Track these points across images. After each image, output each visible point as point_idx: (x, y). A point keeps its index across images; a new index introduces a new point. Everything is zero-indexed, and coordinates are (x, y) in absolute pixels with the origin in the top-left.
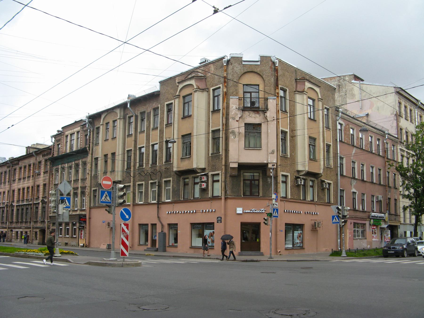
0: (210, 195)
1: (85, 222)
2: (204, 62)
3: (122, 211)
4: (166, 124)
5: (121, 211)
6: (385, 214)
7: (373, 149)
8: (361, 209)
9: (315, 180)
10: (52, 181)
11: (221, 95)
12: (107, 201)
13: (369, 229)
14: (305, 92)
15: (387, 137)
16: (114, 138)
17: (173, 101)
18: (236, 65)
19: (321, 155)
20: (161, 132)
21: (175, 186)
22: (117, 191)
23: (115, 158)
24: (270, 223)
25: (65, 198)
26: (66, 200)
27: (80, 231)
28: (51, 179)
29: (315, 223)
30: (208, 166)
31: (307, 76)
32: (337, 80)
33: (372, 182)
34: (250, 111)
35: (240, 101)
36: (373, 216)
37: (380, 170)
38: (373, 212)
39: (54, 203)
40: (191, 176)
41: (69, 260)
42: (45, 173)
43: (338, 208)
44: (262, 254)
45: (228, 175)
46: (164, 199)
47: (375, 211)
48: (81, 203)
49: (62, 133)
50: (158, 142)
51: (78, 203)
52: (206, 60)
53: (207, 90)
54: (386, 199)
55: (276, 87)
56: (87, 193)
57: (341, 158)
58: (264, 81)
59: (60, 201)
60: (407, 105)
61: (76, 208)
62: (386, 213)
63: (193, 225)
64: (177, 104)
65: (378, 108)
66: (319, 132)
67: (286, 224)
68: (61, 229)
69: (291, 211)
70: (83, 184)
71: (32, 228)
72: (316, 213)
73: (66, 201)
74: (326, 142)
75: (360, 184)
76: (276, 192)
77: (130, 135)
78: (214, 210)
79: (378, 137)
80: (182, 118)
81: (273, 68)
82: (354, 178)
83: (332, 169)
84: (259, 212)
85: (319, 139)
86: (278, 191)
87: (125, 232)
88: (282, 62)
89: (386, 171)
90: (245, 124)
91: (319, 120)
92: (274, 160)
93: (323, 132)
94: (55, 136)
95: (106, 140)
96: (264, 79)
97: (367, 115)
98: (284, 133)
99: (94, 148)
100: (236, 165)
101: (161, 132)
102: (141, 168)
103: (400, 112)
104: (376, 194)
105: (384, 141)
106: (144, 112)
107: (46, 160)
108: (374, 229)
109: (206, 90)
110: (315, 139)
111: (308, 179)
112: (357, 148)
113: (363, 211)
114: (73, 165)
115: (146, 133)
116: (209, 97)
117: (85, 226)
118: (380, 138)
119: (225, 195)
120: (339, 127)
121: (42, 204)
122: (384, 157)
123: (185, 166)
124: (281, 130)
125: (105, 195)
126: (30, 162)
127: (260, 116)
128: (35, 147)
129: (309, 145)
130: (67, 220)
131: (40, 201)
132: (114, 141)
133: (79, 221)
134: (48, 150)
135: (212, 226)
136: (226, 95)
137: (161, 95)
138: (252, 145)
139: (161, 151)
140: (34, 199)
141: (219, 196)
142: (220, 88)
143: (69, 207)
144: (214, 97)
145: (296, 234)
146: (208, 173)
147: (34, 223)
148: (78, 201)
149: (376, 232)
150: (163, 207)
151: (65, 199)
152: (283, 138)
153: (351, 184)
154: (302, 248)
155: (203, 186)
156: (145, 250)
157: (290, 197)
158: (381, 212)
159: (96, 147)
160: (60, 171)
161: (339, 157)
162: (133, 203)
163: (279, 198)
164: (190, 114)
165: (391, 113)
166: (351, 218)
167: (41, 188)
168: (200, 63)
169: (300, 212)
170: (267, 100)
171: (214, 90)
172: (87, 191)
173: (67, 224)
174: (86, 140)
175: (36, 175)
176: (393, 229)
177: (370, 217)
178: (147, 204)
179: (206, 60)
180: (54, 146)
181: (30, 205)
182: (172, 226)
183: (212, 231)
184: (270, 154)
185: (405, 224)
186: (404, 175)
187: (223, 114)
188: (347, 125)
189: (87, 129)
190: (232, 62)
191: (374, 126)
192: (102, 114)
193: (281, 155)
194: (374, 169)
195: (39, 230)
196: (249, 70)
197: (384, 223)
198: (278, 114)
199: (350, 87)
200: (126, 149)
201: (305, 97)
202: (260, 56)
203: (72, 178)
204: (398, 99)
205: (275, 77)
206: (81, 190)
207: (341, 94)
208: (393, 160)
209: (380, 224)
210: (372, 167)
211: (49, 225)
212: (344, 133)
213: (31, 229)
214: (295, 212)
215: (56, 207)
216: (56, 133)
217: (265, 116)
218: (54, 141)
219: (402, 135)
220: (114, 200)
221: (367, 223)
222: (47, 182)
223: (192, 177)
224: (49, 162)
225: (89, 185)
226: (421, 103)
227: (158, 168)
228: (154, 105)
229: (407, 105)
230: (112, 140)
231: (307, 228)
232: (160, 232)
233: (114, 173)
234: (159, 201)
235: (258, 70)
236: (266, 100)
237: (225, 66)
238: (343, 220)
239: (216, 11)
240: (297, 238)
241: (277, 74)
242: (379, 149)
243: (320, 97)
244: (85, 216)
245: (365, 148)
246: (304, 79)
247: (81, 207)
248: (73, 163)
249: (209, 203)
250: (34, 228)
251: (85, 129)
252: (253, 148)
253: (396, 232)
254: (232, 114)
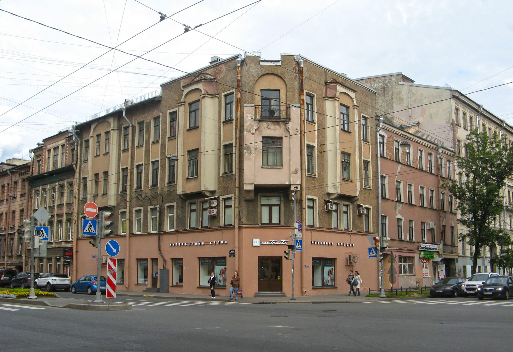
0: (222, 224)
1: (71, 256)
2: (215, 61)
3: (108, 244)
4: (169, 136)
5: (108, 244)
6: (438, 245)
7: (424, 167)
8: (408, 239)
9: (349, 205)
10: (31, 206)
11: (234, 102)
12: (91, 232)
13: (419, 264)
14: (336, 98)
15: (440, 152)
16: (106, 154)
17: (177, 109)
18: (253, 65)
19: (356, 173)
20: (163, 146)
21: (179, 212)
22: (103, 220)
23: (107, 178)
24: (291, 256)
25: (41, 228)
26: (43, 230)
27: (65, 268)
28: (30, 204)
29: (350, 256)
30: (219, 189)
31: (340, 79)
32: (381, 82)
33: (422, 206)
34: (268, 122)
35: (257, 109)
36: (423, 248)
37: (432, 191)
38: (424, 242)
39: (28, 234)
40: (198, 201)
41: (46, 302)
42: (22, 195)
43: (375, 239)
44: (284, 295)
45: (242, 200)
46: (167, 228)
47: (426, 241)
48: (66, 233)
49: (44, 146)
50: (159, 159)
51: (62, 233)
52: (217, 59)
53: (218, 96)
54: (440, 227)
55: (300, 93)
56: (74, 222)
57: (383, 177)
58: (286, 85)
59: (36, 231)
60: (466, 111)
61: (60, 239)
62: (440, 243)
63: (202, 260)
64: (183, 113)
65: (431, 115)
66: (355, 147)
67: (314, 259)
68: (42, 265)
69: (320, 243)
70: (68, 209)
71: (6, 264)
72: (351, 245)
73: (44, 232)
74: (363, 159)
75: (407, 208)
76: (301, 220)
77: (125, 150)
78: (226, 242)
79: (429, 151)
80: (188, 130)
81: (297, 69)
82: (399, 201)
83: (371, 191)
84: (280, 243)
85: (355, 154)
86: (303, 219)
87: (112, 268)
88: (308, 61)
89: (440, 193)
90: (263, 137)
91: (355, 132)
92: (298, 181)
93: (360, 146)
94: (34, 151)
95: (97, 156)
96: (286, 83)
97: (417, 124)
98: (310, 147)
99: (82, 166)
100: (251, 188)
101: (163, 146)
102: (139, 190)
103: (457, 121)
104: (428, 221)
105: (437, 156)
106: (143, 122)
107: (24, 180)
108: (425, 264)
109: (217, 96)
110: (349, 155)
111: (341, 203)
112: (403, 165)
113: (410, 242)
114: (57, 187)
115: (145, 148)
116: (220, 105)
117: (71, 261)
118: (432, 152)
119: (239, 223)
120: (379, 139)
121: (19, 234)
122: (437, 176)
123: (191, 188)
124: (307, 144)
125: (88, 225)
126: (4, 182)
127: (281, 127)
128: (11, 163)
129: (342, 161)
130: (44, 254)
131: (15, 231)
132: (106, 157)
133: (64, 255)
134: (26, 167)
135: (224, 261)
136: (240, 101)
137: (162, 102)
138: (271, 162)
139: (163, 169)
140: (9, 228)
141: (231, 225)
142: (232, 93)
143: (47, 239)
144: (226, 104)
145: (327, 269)
146: (218, 197)
147: (8, 258)
148: (63, 231)
149: (428, 266)
150: (165, 238)
151: (42, 229)
152: (310, 154)
153: (396, 209)
154: (333, 287)
155: (213, 212)
156: (144, 291)
157: (318, 226)
158: (433, 243)
159: (85, 164)
160: (40, 193)
161: (380, 177)
162: (130, 233)
163: (304, 227)
164: (197, 125)
165: (446, 122)
166: (395, 250)
167: (18, 215)
168: (211, 63)
169: (331, 244)
170: (290, 108)
171: (226, 96)
172: (74, 218)
173: (41, 259)
174: (73, 155)
175: (11, 199)
176: (449, 263)
177: (420, 249)
178: (146, 234)
179: (217, 59)
180: (33, 162)
181: (3, 236)
182: (177, 262)
183: (223, 267)
184: (293, 173)
185: (464, 256)
186: (461, 197)
187: (236, 126)
188: (390, 137)
189: (73, 142)
190: (247, 63)
191: (424, 137)
192: (92, 124)
193: (306, 175)
194: (425, 190)
195: (14, 266)
196: (268, 72)
197: (437, 256)
198: (303, 126)
199: (397, 90)
200: (121, 168)
201: (337, 104)
202: (282, 55)
203: (55, 203)
204: (455, 105)
205: (300, 81)
206: (67, 218)
207: (386, 98)
208: (449, 179)
209: (433, 258)
210: (422, 188)
211: (28, 260)
212: (386, 147)
213: (4, 265)
214: (324, 243)
215: (32, 239)
216: (35, 146)
217: (287, 128)
218: (34, 156)
219: (460, 149)
220: (100, 231)
221: (416, 256)
222: (24, 207)
223: (200, 201)
224: (27, 183)
225: (76, 211)
226: (483, 109)
227: (159, 191)
228: (155, 114)
229: (466, 111)
230: (104, 156)
231: (340, 263)
232: (162, 268)
233: (106, 197)
234: (159, 231)
235: (279, 72)
236: (288, 108)
237: (239, 67)
238: (381, 253)
239: (187, 30)
240: (328, 275)
241: (302, 76)
242: (430, 166)
243: (355, 104)
244: (71, 249)
245: (413, 164)
246: (335, 82)
247: (66, 238)
248: (57, 184)
249: (219, 233)
250: (8, 264)
251: (71, 142)
252: (272, 167)
253: (453, 267)
254: (247, 125)
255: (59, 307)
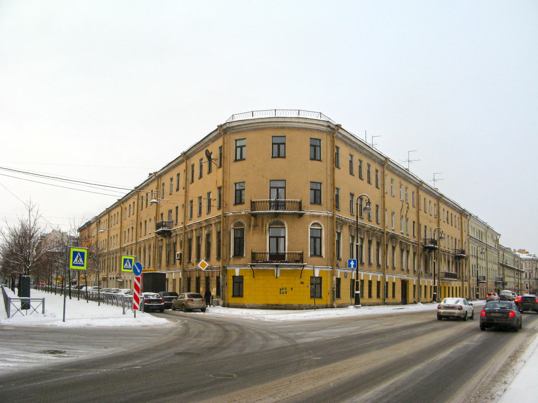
12: (79, 263)
61: (357, 290)
255: (425, 231)
